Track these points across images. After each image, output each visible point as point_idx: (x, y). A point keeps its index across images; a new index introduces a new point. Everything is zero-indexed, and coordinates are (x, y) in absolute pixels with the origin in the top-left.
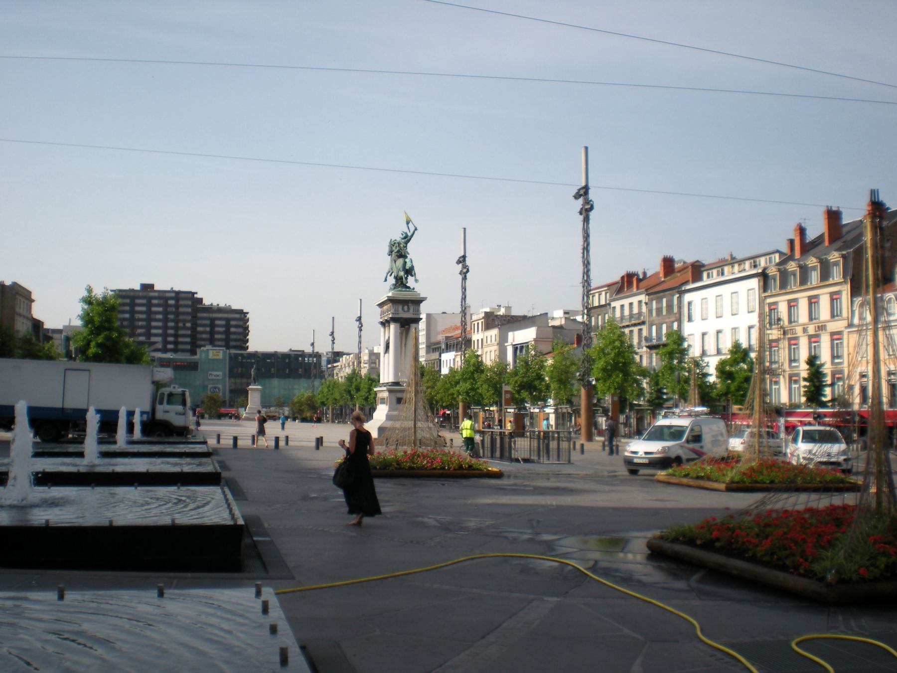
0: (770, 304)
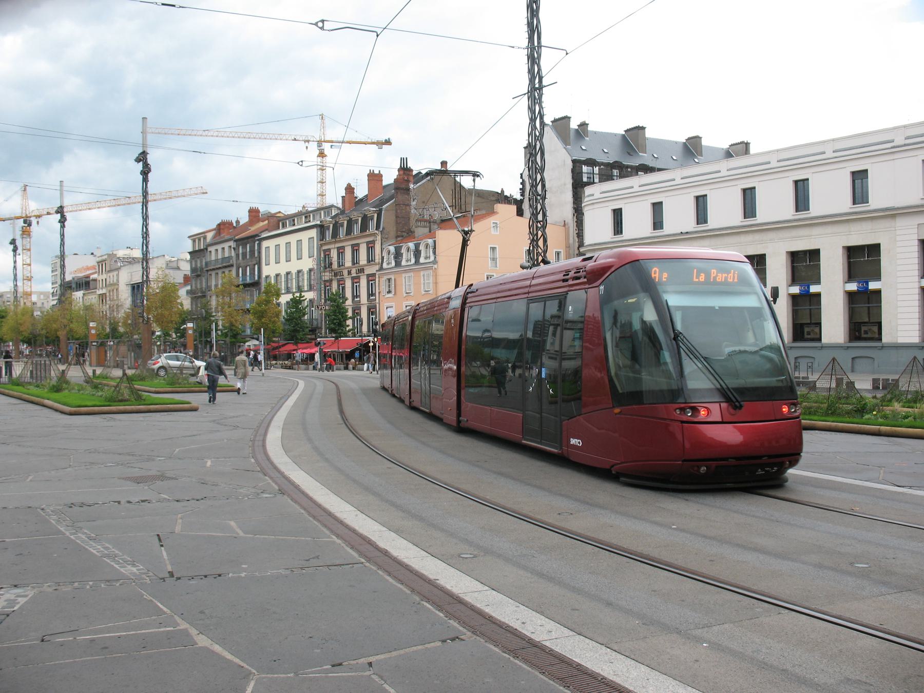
0: (325, 251)
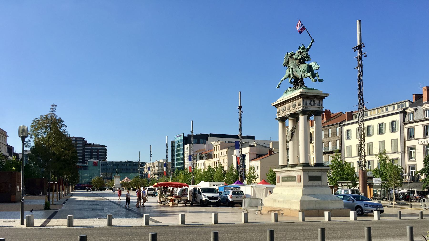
0: (409, 129)
